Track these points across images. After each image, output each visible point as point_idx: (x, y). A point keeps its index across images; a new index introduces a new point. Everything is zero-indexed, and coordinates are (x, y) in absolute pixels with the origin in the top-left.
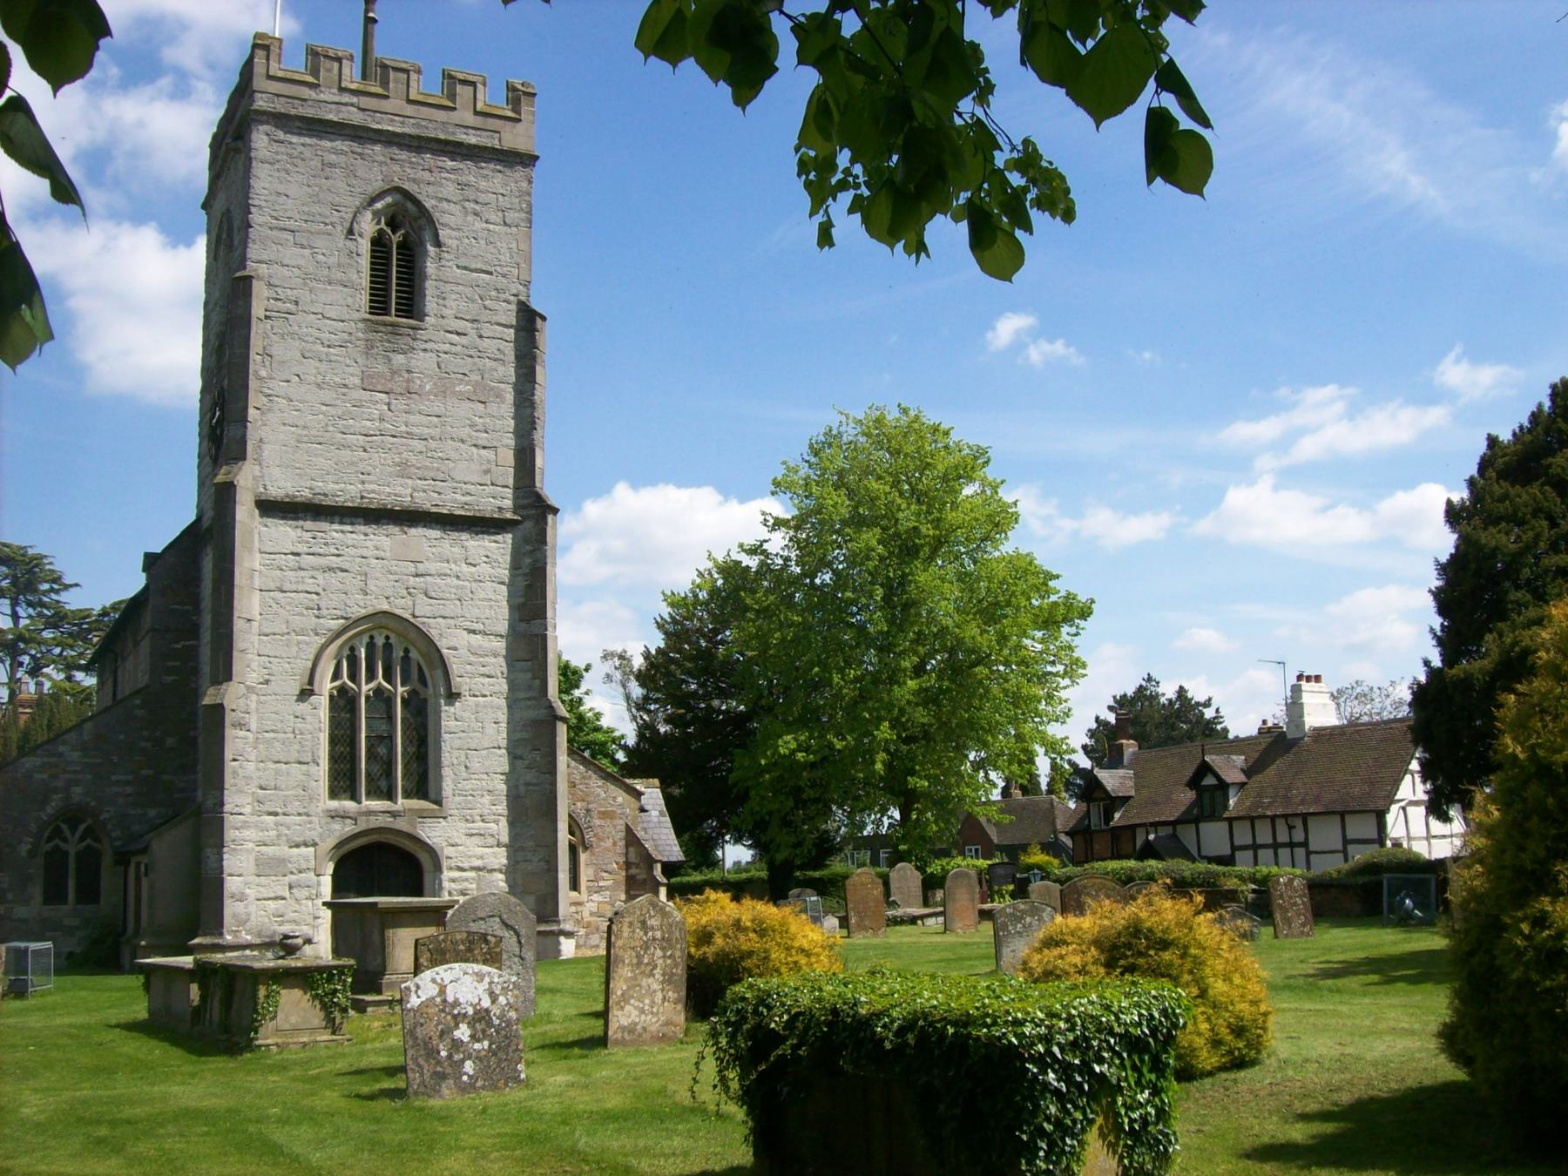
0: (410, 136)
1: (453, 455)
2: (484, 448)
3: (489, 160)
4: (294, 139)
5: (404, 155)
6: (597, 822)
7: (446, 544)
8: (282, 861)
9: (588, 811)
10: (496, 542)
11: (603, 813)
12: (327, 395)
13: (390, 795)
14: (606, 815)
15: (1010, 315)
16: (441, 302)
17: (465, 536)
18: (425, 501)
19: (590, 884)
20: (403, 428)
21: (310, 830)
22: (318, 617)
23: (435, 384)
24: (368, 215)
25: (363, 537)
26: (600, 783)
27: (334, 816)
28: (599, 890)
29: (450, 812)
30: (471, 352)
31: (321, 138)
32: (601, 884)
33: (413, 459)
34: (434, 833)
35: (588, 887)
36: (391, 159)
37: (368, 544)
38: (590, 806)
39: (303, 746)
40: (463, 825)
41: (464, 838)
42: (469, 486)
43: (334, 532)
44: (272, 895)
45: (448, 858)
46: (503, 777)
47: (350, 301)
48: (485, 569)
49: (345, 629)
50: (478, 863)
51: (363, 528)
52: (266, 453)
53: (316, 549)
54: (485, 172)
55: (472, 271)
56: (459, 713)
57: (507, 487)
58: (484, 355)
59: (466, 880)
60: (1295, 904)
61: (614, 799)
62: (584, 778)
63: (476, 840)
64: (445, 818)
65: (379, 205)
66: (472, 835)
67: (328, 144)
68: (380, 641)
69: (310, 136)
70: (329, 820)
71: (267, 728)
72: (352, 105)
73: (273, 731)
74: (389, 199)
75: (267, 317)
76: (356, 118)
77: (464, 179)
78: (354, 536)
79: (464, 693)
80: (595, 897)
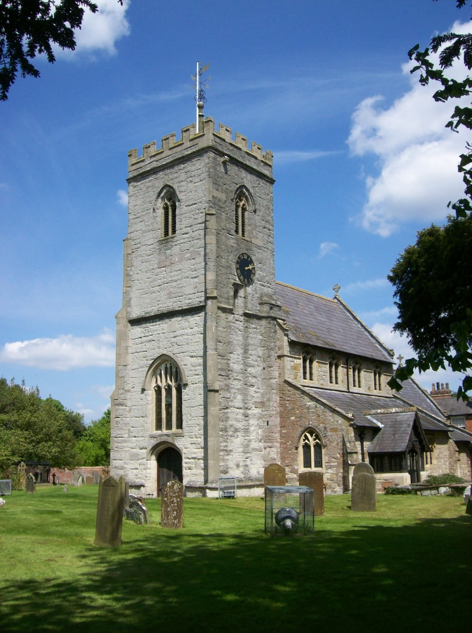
0: (169, 163)
1: (185, 284)
2: (195, 278)
3: (194, 158)
4: (139, 183)
5: (168, 171)
6: (330, 433)
7: (183, 322)
8: (137, 455)
9: (325, 428)
10: (199, 316)
11: (332, 429)
12: (149, 274)
13: (161, 429)
14: (334, 430)
15: (355, 114)
16: (181, 223)
17: (189, 317)
18: (176, 306)
19: (327, 464)
20: (170, 279)
21: (144, 442)
22: (147, 360)
23: (179, 257)
24: (160, 200)
25: (159, 326)
26: (331, 414)
27: (152, 437)
28: (331, 467)
29: (185, 434)
30: (190, 239)
31: (145, 179)
32: (332, 464)
33: (172, 290)
34: (179, 443)
35: (326, 466)
36: (165, 175)
37: (160, 328)
38: (326, 426)
39: (143, 410)
40: (189, 439)
41: (190, 445)
42: (190, 296)
43: (151, 326)
44: (135, 468)
45: (185, 453)
46: (203, 418)
47: (154, 235)
48: (196, 329)
49: (153, 363)
50: (194, 456)
51: (158, 323)
52: (132, 302)
53: (146, 334)
54: (194, 163)
55: (190, 206)
56: (188, 392)
57: (202, 292)
58: (194, 239)
59: (190, 463)
60: (173, 502)
61: (337, 421)
62: (323, 412)
63: (194, 446)
64: (183, 437)
65: (162, 195)
66: (192, 444)
67: (147, 180)
68: (168, 366)
69: (143, 180)
70: (150, 438)
71: (133, 405)
72: (154, 161)
73: (135, 406)
74: (165, 191)
75: (133, 252)
76: (155, 165)
77: (186, 170)
78: (156, 326)
79: (189, 383)
80: (329, 471)
